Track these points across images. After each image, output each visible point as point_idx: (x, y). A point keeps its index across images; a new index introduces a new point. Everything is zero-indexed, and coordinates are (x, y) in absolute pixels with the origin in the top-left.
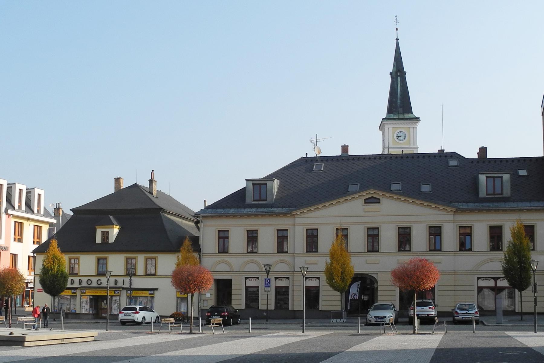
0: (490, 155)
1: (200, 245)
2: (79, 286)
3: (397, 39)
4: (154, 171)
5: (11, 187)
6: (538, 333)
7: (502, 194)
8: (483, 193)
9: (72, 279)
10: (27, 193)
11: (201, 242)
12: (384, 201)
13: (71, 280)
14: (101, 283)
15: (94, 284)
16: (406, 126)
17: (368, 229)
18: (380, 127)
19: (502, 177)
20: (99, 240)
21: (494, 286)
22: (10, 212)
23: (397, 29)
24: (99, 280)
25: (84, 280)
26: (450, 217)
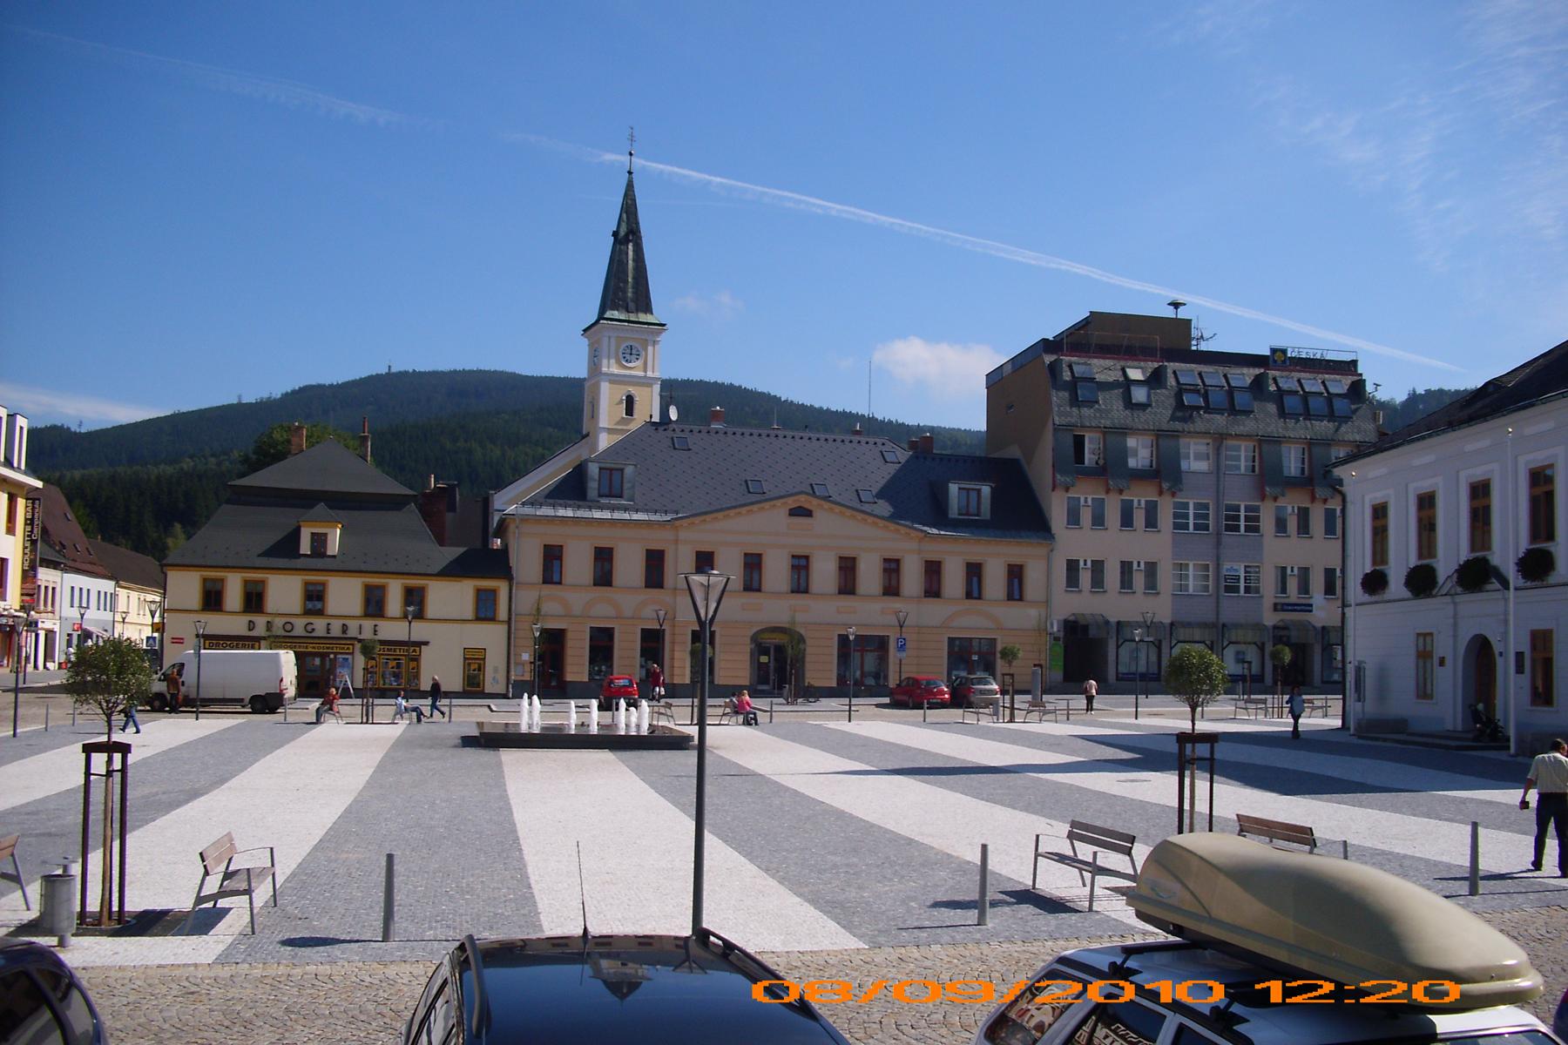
2: (268, 634)
6: (853, 722)
7: (978, 515)
8: (953, 512)
9: (253, 622)
12: (817, 513)
14: (313, 630)
15: (299, 631)
20: (305, 547)
21: (93, 755)
24: (308, 624)
25: (279, 622)
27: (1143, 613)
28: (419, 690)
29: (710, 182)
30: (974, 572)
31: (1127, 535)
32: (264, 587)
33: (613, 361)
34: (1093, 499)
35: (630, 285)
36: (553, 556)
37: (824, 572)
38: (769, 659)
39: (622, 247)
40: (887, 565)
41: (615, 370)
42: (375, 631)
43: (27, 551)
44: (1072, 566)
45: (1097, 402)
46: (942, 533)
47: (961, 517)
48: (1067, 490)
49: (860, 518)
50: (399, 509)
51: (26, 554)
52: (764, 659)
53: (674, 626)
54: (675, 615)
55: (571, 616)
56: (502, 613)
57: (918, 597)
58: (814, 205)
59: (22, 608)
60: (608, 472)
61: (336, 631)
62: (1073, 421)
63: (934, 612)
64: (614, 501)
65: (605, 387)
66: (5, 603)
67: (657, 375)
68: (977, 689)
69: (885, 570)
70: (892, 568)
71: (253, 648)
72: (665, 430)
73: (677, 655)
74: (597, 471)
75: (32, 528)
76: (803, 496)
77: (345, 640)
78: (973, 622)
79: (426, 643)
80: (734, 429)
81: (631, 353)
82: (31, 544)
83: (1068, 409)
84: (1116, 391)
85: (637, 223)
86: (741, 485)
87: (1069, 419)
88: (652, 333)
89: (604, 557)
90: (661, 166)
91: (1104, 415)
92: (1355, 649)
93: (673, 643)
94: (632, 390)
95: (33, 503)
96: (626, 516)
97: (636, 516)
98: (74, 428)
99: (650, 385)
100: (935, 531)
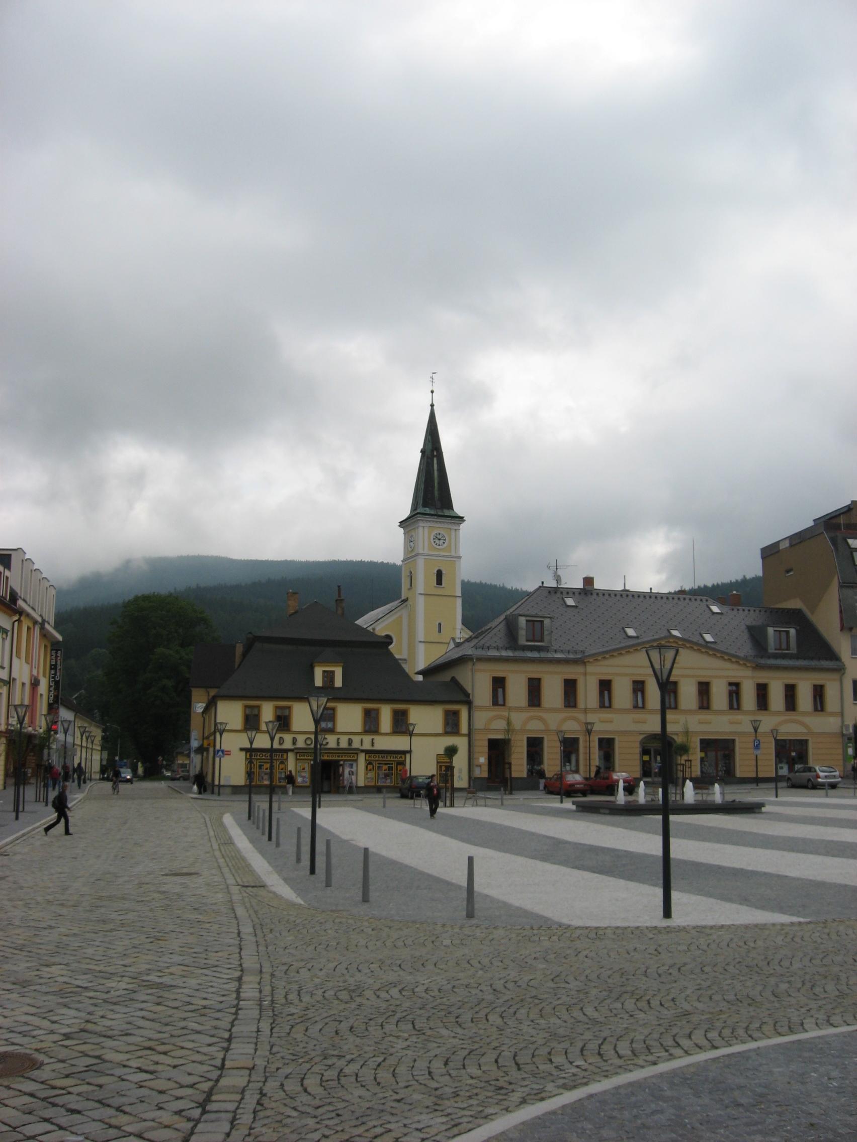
0: (598, 585)
3: (432, 406)
7: (787, 650)
13: (280, 738)
14: (327, 743)
16: (446, 526)
20: (319, 682)
23: (432, 392)
26: (749, 673)
30: (790, 692)
32: (259, 711)
38: (650, 758)
40: (730, 688)
43: (52, 689)
47: (777, 651)
51: (51, 691)
56: (464, 729)
61: (344, 744)
70: (735, 691)
74: (524, 622)
77: (352, 753)
82: (55, 684)
92: (590, 747)
95: (56, 653)
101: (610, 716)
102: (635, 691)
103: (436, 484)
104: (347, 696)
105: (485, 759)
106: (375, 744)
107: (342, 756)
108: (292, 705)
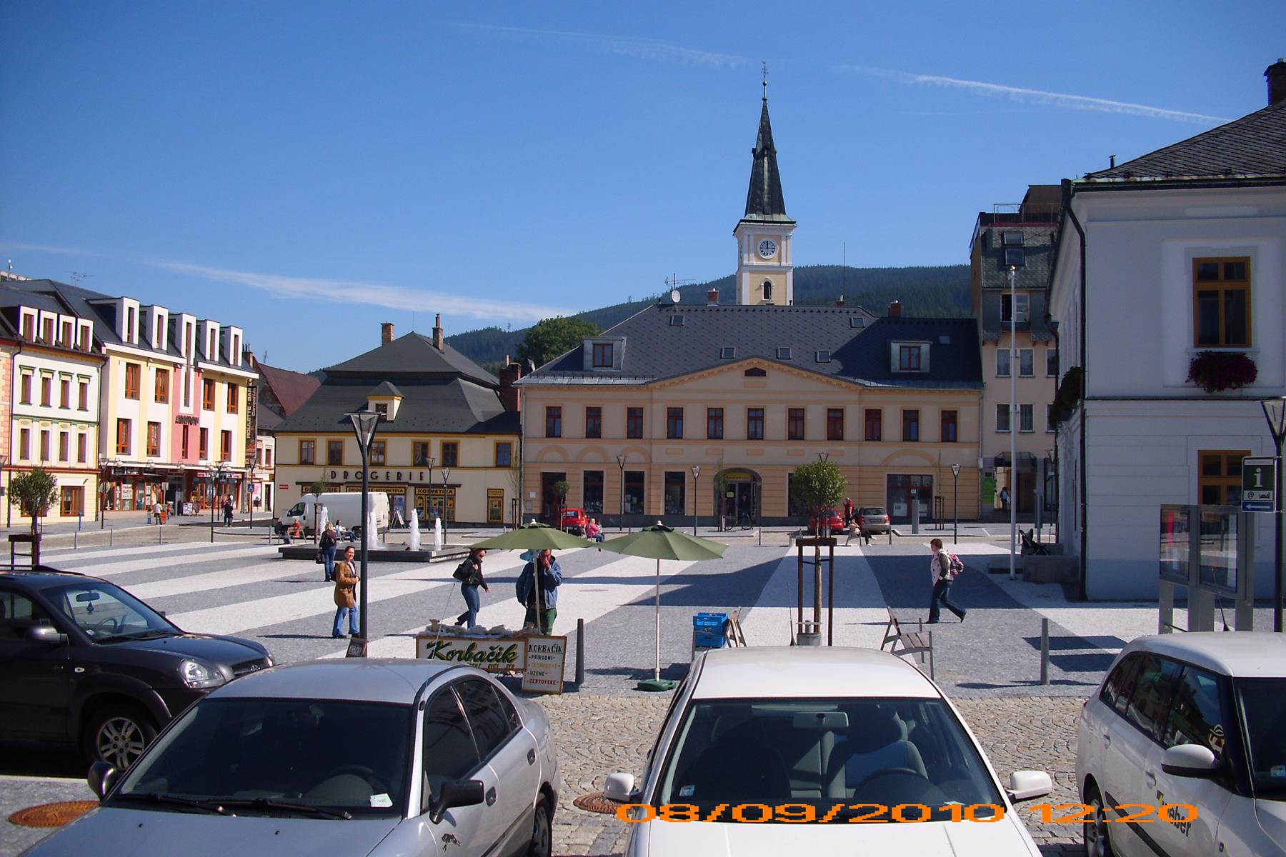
1: (521, 426)
2: (345, 481)
4: (440, 316)
5: (146, 312)
6: (957, 544)
7: (919, 369)
8: (895, 366)
10: (221, 333)
11: (522, 422)
14: (377, 477)
17: (749, 409)
18: (734, 231)
19: (919, 348)
22: (201, 365)
23: (764, 84)
25: (352, 472)
27: (1048, 451)
28: (454, 522)
29: (1008, 93)
31: (1027, 382)
33: (752, 255)
34: (1021, 351)
35: (766, 191)
36: (553, 415)
37: (776, 422)
39: (759, 161)
41: (754, 262)
42: (421, 477)
43: (249, 425)
44: (1004, 411)
45: (1024, 265)
46: (879, 385)
48: (997, 344)
49: (687, 379)
50: (447, 384)
52: (730, 495)
53: (650, 469)
54: (651, 458)
55: (567, 463)
57: (859, 441)
58: (1100, 104)
59: (247, 466)
60: (601, 347)
61: (393, 478)
62: (999, 283)
63: (874, 453)
64: (604, 370)
65: (746, 276)
66: (206, 461)
67: (790, 264)
68: (867, 518)
69: (829, 419)
71: (335, 491)
72: (668, 310)
73: (653, 492)
75: (252, 408)
76: (755, 359)
78: (911, 461)
79: (459, 486)
80: (812, 308)
81: (767, 247)
83: (995, 273)
84: (1042, 255)
85: (771, 140)
86: (716, 352)
87: (996, 281)
88: (784, 229)
89: (594, 415)
90: (966, 83)
91: (1029, 277)
93: (650, 482)
94: (770, 278)
96: (611, 381)
97: (618, 381)
98: (504, 329)
99: (784, 273)
100: (874, 384)
101: (842, 448)
102: (906, 420)
103: (766, 183)
104: (398, 429)
105: (536, 494)
106: (390, 478)
107: (390, 491)
108: (316, 439)
